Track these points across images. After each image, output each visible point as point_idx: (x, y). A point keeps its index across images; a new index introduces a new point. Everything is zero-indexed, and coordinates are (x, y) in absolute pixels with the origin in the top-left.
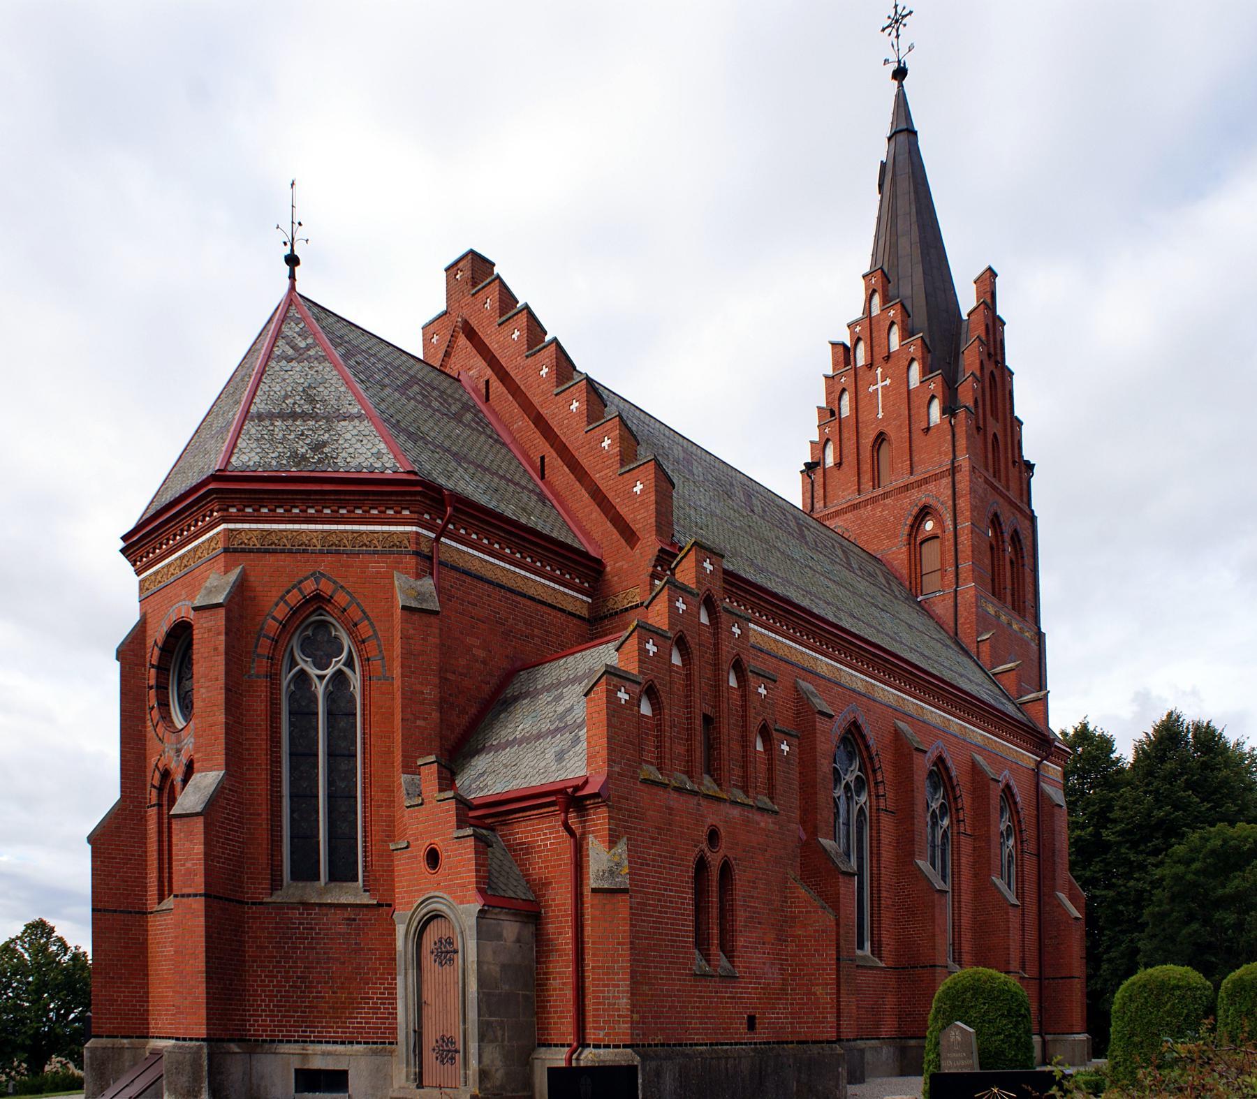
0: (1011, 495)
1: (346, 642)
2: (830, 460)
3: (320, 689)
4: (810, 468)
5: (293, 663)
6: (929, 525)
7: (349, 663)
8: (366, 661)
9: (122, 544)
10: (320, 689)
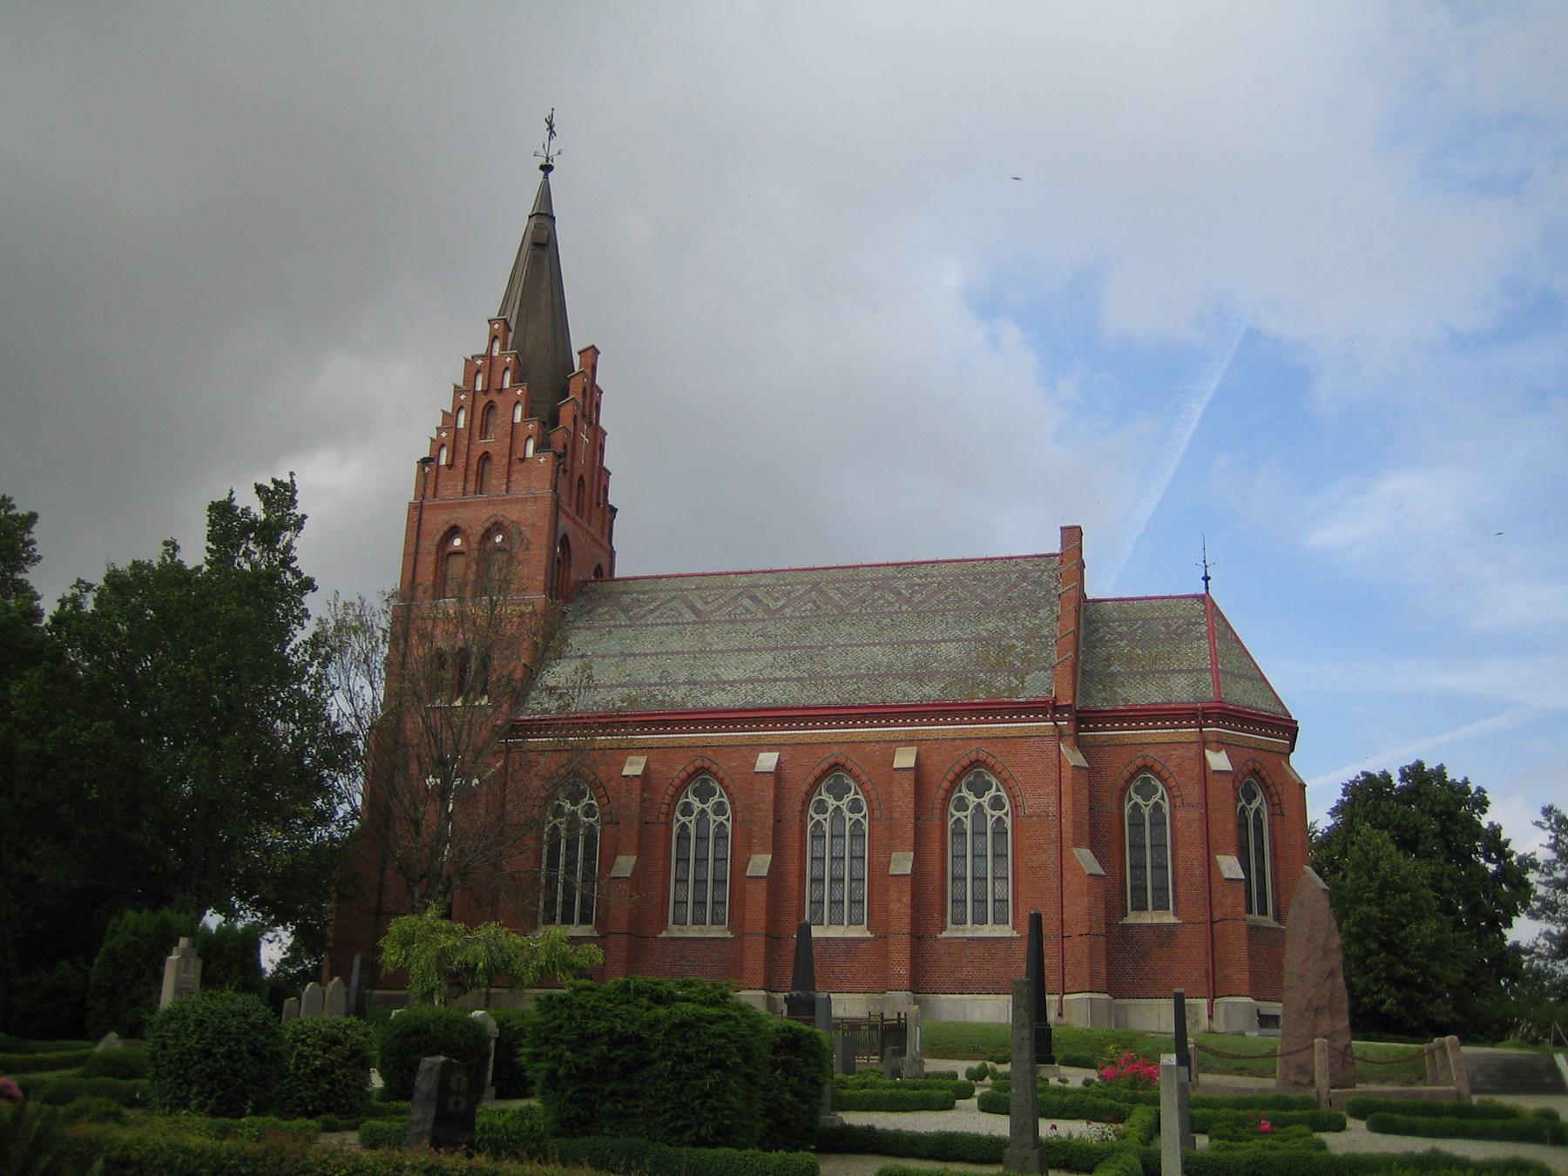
0: (593, 531)
1: (1161, 788)
2: (443, 461)
3: (1146, 812)
4: (424, 462)
5: (1130, 799)
6: (457, 542)
7: (1162, 798)
8: (1172, 798)
9: (1430, 765)
10: (1146, 812)
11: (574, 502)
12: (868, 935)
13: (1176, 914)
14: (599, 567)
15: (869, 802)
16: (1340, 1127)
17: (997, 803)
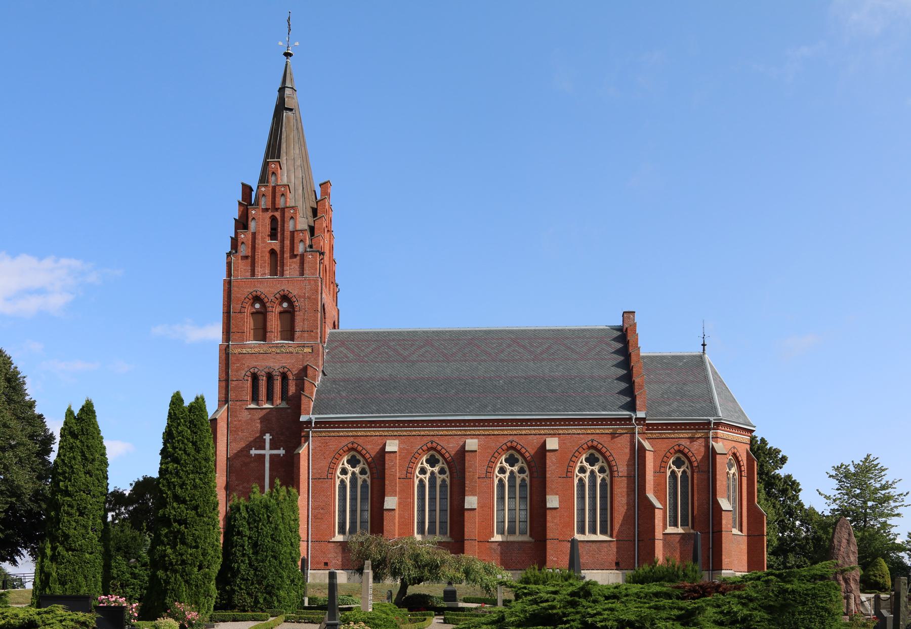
3: (679, 475)
12: (531, 539)
17: (602, 470)
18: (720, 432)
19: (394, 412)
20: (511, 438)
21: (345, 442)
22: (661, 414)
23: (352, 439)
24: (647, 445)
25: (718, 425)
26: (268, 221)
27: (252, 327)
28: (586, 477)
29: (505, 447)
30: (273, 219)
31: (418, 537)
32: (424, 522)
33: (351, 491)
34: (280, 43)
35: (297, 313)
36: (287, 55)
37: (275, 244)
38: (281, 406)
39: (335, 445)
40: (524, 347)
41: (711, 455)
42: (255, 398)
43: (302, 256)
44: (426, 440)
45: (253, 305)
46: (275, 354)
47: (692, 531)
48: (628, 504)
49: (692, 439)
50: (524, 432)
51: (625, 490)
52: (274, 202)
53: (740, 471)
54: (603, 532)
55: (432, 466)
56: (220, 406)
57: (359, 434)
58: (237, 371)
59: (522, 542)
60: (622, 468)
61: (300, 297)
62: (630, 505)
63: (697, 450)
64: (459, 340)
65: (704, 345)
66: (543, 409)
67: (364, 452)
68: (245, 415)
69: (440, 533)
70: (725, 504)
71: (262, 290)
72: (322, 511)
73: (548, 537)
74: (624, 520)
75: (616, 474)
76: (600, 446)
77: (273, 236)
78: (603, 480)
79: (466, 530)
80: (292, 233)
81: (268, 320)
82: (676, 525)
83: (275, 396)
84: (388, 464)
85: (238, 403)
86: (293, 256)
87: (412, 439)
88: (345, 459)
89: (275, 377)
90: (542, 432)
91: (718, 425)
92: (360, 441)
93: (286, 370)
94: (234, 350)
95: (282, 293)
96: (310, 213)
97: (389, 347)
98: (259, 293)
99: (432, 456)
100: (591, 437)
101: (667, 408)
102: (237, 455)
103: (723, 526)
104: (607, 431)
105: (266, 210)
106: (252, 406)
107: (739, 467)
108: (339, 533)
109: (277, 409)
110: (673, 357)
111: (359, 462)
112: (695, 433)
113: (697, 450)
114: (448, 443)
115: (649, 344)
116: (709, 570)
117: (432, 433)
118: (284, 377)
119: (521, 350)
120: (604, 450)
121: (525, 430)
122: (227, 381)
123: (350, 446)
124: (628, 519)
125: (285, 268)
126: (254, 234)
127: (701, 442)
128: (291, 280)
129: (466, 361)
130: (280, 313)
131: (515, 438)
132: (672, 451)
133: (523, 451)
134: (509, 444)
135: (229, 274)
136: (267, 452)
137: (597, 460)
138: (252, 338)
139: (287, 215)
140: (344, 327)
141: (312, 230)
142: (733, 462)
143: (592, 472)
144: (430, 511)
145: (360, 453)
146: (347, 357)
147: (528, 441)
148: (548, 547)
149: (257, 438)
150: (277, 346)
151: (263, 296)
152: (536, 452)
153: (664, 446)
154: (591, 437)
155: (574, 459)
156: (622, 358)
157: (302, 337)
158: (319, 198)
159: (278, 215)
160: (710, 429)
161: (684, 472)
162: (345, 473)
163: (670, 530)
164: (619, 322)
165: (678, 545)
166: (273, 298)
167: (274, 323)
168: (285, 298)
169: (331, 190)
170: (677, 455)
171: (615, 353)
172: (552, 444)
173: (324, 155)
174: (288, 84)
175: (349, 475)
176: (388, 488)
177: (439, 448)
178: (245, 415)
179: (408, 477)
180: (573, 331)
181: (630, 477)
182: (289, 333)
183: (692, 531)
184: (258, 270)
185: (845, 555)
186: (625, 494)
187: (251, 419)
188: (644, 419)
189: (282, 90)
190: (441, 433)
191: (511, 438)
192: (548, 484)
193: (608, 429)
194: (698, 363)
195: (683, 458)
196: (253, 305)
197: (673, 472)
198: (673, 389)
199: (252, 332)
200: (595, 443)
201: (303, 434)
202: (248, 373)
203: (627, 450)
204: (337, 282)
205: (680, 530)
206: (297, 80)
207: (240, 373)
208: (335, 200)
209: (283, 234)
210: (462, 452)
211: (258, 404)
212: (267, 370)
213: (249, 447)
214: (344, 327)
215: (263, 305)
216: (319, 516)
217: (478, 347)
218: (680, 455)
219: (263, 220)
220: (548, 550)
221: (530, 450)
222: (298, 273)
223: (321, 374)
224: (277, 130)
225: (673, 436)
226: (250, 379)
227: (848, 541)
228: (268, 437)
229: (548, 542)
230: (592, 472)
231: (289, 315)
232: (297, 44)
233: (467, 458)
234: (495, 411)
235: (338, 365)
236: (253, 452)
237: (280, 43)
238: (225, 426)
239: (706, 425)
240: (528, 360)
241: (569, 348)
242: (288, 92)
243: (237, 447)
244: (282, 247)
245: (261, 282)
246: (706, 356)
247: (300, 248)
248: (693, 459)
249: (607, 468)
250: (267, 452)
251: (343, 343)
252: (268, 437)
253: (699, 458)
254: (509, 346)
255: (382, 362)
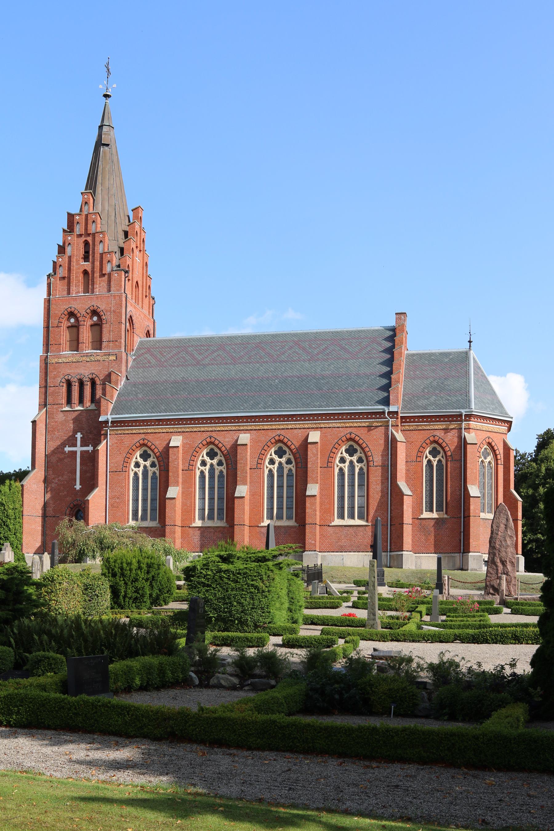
3: (435, 464)
5: (426, 457)
10: (435, 464)
11: (134, 298)
12: (296, 524)
13: (446, 513)
14: (148, 331)
15: (296, 459)
16: (497, 612)
17: (360, 460)
18: (473, 424)
19: (180, 410)
20: (278, 432)
21: (137, 438)
22: (418, 407)
23: (143, 436)
24: (399, 436)
25: (469, 417)
26: (82, 246)
27: (68, 339)
28: (346, 467)
29: (273, 441)
30: (86, 243)
31: (132, 523)
32: (272, 509)
33: (143, 482)
34: (101, 86)
35: (104, 326)
36: (106, 96)
37: (87, 266)
38: (90, 408)
39: (129, 441)
40: (304, 349)
41: (463, 444)
42: (69, 401)
43: (109, 275)
44: (205, 435)
45: (68, 319)
46: (84, 363)
47: (446, 516)
48: (382, 491)
49: (446, 430)
50: (290, 427)
51: (380, 478)
52: (86, 229)
53: (497, 460)
54: (361, 517)
55: (351, 455)
56: (40, 410)
57: (149, 431)
58: (54, 379)
59: (288, 526)
60: (377, 458)
61: (107, 311)
62: (384, 493)
63: (450, 440)
64: (248, 343)
65: (470, 342)
66: (308, 405)
67: (153, 447)
68: (60, 417)
69: (218, 519)
70: (474, 490)
71: (75, 307)
72: (117, 500)
73: (307, 522)
74: (378, 506)
75: (371, 464)
76: (357, 439)
77: (86, 258)
78: (361, 469)
79: (236, 516)
80: (101, 255)
81: (80, 332)
82: (431, 511)
83: (85, 399)
84: (172, 457)
85: (55, 406)
86: (102, 275)
87: (193, 435)
88: (138, 454)
89: (85, 383)
90: (306, 426)
91: (469, 417)
92: (150, 437)
93: (94, 376)
94: (52, 360)
95: (92, 308)
96: (122, 235)
97: (187, 352)
98: (73, 309)
99: (212, 450)
100: (349, 430)
101: (425, 402)
102: (54, 452)
103: (471, 511)
104: (364, 425)
105: (81, 235)
106: (67, 409)
107: (495, 455)
108: (133, 519)
109: (87, 411)
110: (441, 354)
111: (149, 456)
112: (449, 425)
113: (450, 440)
114: (225, 438)
115: (414, 343)
116: (460, 553)
117: (210, 429)
118: (93, 383)
119: (300, 352)
120: (361, 442)
121: (291, 425)
122: (46, 387)
123: (141, 442)
124: (382, 505)
125: (95, 286)
126: (70, 257)
127: (454, 433)
128: (100, 297)
129: (250, 363)
130: (91, 326)
131: (282, 432)
132: (428, 441)
133: (289, 443)
134: (277, 438)
135: (49, 294)
136: (79, 449)
137: (355, 451)
138: (68, 348)
139: (97, 239)
140: (161, 334)
141: (122, 250)
142: (489, 451)
143: (351, 462)
144: (278, 497)
145: (285, 444)
146: (149, 362)
147: (293, 434)
148: (307, 531)
149: (70, 436)
150: (87, 355)
151: (76, 312)
152: (300, 445)
153: (419, 438)
154: (349, 430)
155: (334, 450)
156: (388, 356)
157: (108, 347)
158: (131, 221)
159: (89, 239)
160: (461, 421)
161: (439, 461)
162: (137, 466)
163: (426, 515)
164: (392, 323)
165: (432, 529)
166: (84, 313)
167: (86, 334)
168: (95, 313)
169: (141, 214)
170: (433, 445)
171: (382, 351)
172: (314, 437)
173: (136, 181)
174: (106, 123)
175: (276, 465)
176: (171, 479)
177: (217, 442)
178: (60, 417)
179: (189, 469)
180: (350, 333)
181: (384, 467)
182: (98, 344)
183: (446, 516)
184: (73, 288)
185: (502, 539)
186: (379, 482)
187: (65, 420)
188: (397, 413)
189: (101, 127)
190: (218, 429)
191: (278, 432)
192: (309, 474)
193: (365, 423)
194: (463, 358)
195: (439, 448)
196: (68, 319)
197: (429, 462)
198: (435, 383)
199: (68, 343)
200: (353, 436)
201: (103, 432)
202: (63, 380)
203: (382, 442)
204: (153, 294)
205: (435, 515)
206: (116, 119)
207: (57, 380)
208: (148, 221)
209: (93, 256)
210: (235, 446)
211: (71, 407)
212: (78, 377)
213: (63, 445)
214: (161, 334)
215: (77, 319)
216: (115, 505)
217: (264, 350)
218: (436, 445)
219: (78, 244)
220: (307, 534)
221: (296, 443)
222: (106, 290)
223: (124, 379)
224: (95, 164)
225: (428, 428)
226: (65, 385)
227: (506, 526)
228: (79, 436)
229: (307, 526)
230: (351, 462)
231: (98, 326)
232: (115, 86)
233: (239, 451)
234: (266, 407)
235: (141, 370)
236: (67, 449)
237: (101, 86)
238: (44, 427)
239: (458, 417)
240: (304, 361)
241: (343, 348)
242: (105, 129)
243: (53, 445)
244: (93, 268)
245: (75, 299)
246: (472, 352)
247: (108, 268)
248: (447, 449)
249: (364, 458)
250: (79, 449)
251: (149, 350)
252: (79, 436)
253: (453, 448)
254: (291, 348)
255: (178, 366)
